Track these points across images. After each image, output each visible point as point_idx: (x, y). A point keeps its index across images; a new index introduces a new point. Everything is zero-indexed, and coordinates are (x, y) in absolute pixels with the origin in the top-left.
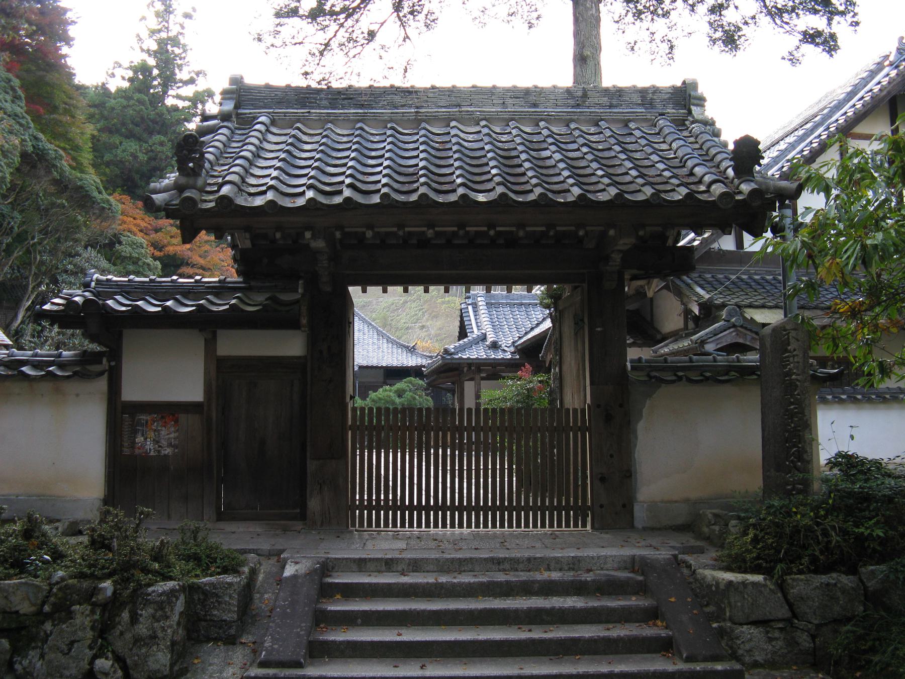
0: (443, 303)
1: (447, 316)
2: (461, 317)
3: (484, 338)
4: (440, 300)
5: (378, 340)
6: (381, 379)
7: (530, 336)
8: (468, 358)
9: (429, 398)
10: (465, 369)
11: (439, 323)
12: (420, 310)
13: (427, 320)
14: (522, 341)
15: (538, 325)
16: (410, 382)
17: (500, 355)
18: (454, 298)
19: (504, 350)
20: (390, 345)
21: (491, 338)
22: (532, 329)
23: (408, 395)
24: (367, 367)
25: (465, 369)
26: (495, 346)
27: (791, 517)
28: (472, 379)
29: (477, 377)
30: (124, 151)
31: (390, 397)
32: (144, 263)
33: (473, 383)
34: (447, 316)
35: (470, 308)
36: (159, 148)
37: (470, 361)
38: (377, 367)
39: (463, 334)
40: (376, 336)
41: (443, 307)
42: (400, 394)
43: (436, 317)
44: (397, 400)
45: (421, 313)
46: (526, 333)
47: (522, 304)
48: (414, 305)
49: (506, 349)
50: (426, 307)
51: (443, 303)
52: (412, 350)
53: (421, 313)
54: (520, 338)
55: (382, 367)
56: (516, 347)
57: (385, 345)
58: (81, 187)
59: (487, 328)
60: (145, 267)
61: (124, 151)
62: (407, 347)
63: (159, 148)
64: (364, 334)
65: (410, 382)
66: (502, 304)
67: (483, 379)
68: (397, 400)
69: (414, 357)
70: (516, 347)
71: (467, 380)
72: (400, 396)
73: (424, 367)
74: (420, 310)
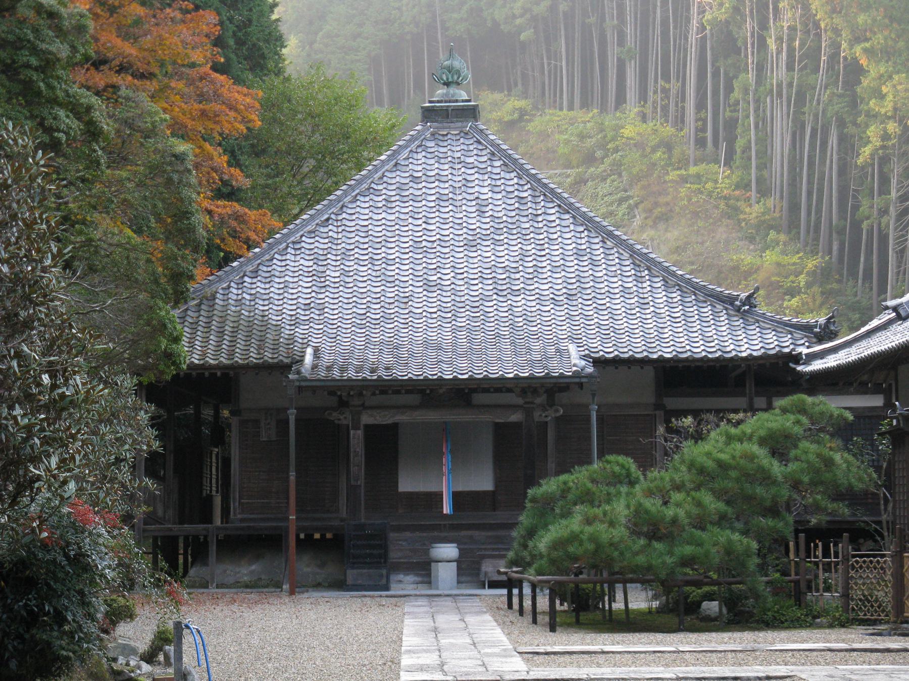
0: (684, 180)
1: (695, 214)
4: (673, 175)
5: (639, 279)
11: (674, 235)
12: (621, 201)
13: (643, 228)
18: (713, 167)
20: (676, 296)
24: (617, 362)
27: (570, 489)
31: (751, 458)
34: (695, 214)
40: (629, 270)
41: (683, 191)
42: (779, 445)
43: (665, 218)
44: (776, 468)
45: (623, 209)
48: (604, 188)
50: (636, 192)
51: (684, 180)
52: (743, 309)
53: (623, 209)
57: (661, 296)
62: (729, 301)
64: (594, 263)
65: (802, 410)
68: (776, 468)
69: (754, 330)
74: (621, 201)
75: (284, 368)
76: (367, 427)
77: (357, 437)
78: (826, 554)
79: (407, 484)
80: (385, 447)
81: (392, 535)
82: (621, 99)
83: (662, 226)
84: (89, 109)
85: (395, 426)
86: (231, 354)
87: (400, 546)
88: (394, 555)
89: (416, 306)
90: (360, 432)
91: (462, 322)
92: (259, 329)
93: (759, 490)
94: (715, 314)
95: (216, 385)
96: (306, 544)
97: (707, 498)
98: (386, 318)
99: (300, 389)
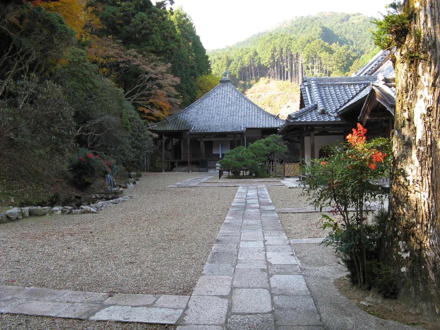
2: (301, 94)
3: (315, 107)
6: (260, 135)
7: (347, 105)
8: (305, 122)
9: (286, 146)
10: (305, 129)
14: (343, 108)
15: (353, 98)
16: (274, 137)
17: (327, 119)
19: (330, 115)
21: (320, 107)
22: (349, 101)
23: (272, 145)
24: (251, 129)
25: (305, 129)
26: (323, 112)
28: (309, 135)
29: (312, 134)
30: (108, 11)
31: (261, 146)
32: (83, 65)
33: (309, 137)
35: (306, 88)
36: (128, 9)
37: (307, 123)
38: (257, 128)
39: (302, 105)
44: (266, 148)
46: (345, 104)
47: (341, 85)
49: (331, 114)
54: (341, 107)
55: (260, 128)
56: (338, 113)
58: (48, 20)
59: (317, 100)
60: (84, 68)
61: (108, 11)
63: (128, 9)
66: (328, 85)
67: (316, 135)
68: (266, 148)
70: (338, 113)
71: (306, 136)
72: (267, 145)
73: (279, 128)
75: (189, 130)
76: (204, 141)
77: (202, 143)
78: (273, 164)
79: (215, 152)
80: (209, 145)
81: (209, 162)
82: (287, 78)
83: (294, 103)
84: (94, 83)
85: (212, 141)
86: (181, 128)
87: (210, 164)
88: (209, 165)
89: (215, 118)
90: (202, 142)
91: (223, 121)
92: (185, 123)
93: (262, 152)
94: (271, 119)
95: (178, 134)
96: (193, 163)
97: (251, 154)
98: (209, 121)
99: (190, 134)
